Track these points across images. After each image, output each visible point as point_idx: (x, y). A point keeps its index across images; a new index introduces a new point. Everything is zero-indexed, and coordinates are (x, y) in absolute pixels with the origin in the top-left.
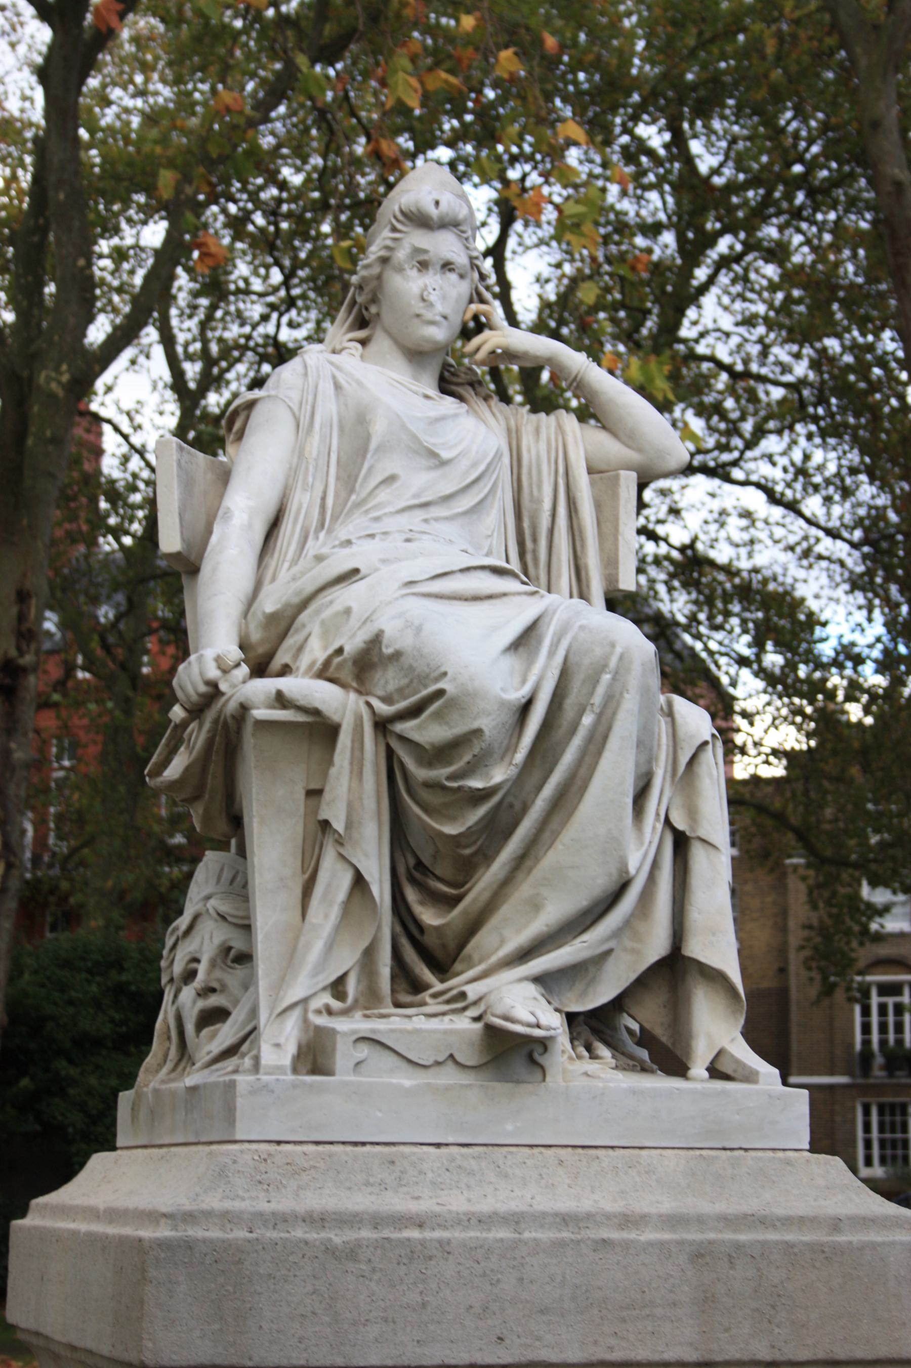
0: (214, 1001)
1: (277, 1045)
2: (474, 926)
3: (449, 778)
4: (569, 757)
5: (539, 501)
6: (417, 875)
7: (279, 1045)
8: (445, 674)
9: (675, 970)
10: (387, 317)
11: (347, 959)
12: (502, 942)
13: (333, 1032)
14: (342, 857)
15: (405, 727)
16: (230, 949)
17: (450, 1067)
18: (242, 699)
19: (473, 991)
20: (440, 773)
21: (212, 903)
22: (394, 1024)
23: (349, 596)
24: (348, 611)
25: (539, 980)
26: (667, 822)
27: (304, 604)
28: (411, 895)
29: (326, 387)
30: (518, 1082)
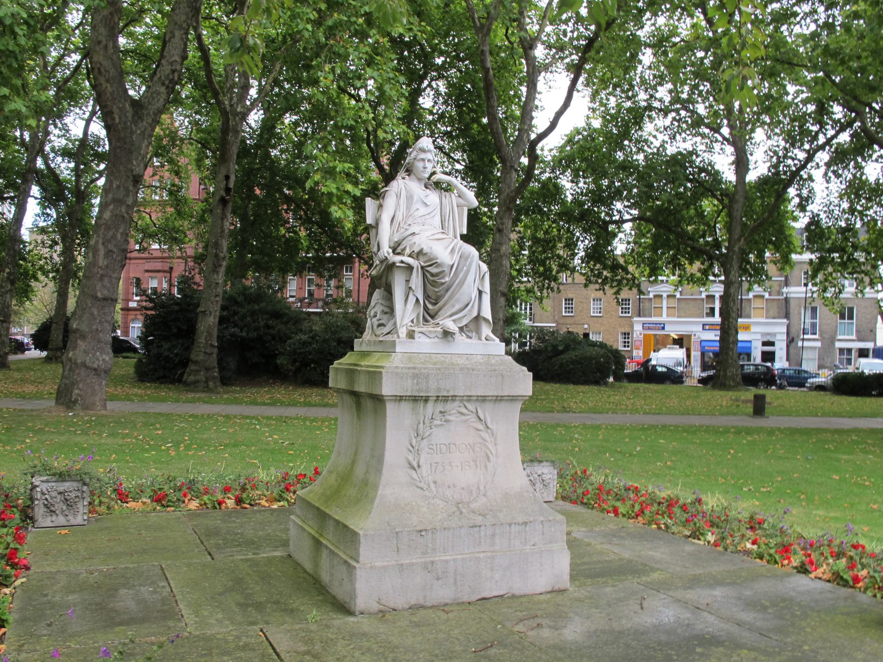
0: (381, 322)
2: (440, 309)
7: (403, 332)
9: (478, 318)
10: (414, 171)
11: (414, 316)
13: (414, 331)
15: (428, 269)
19: (441, 323)
20: (435, 278)
23: (416, 239)
25: (454, 321)
28: (427, 302)
29: (403, 189)
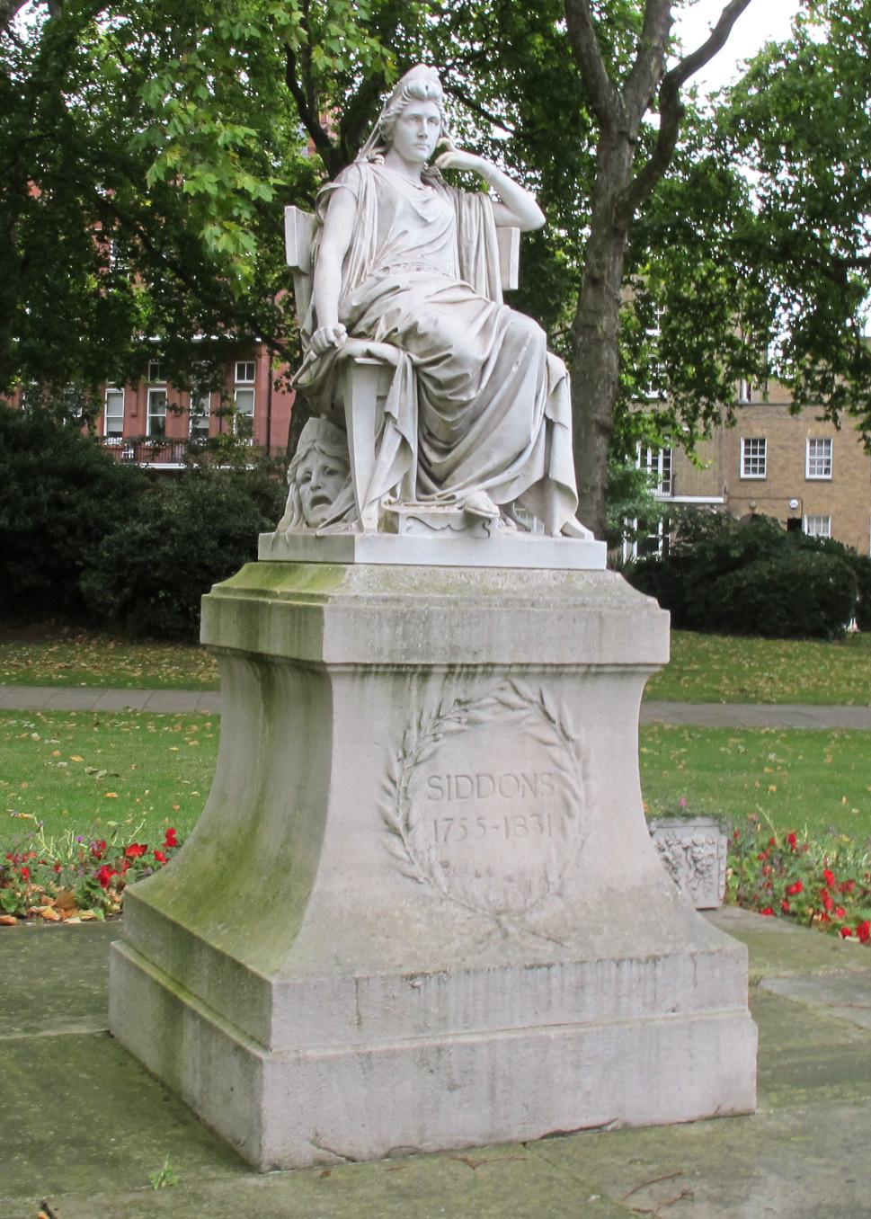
0: (320, 493)
1: (369, 519)
2: (456, 464)
3: (451, 395)
4: (505, 386)
5: (471, 242)
6: (428, 438)
8: (451, 346)
9: (544, 485)
10: (397, 144)
11: (396, 479)
12: (472, 472)
13: (396, 514)
14: (396, 430)
15: (429, 370)
16: (326, 467)
17: (448, 530)
18: (348, 353)
19: (458, 495)
20: (446, 393)
21: (316, 445)
22: (421, 510)
23: (400, 301)
24: (399, 310)
25: (489, 491)
26: (545, 416)
27: (373, 302)
28: (426, 448)
30: (477, 538)
